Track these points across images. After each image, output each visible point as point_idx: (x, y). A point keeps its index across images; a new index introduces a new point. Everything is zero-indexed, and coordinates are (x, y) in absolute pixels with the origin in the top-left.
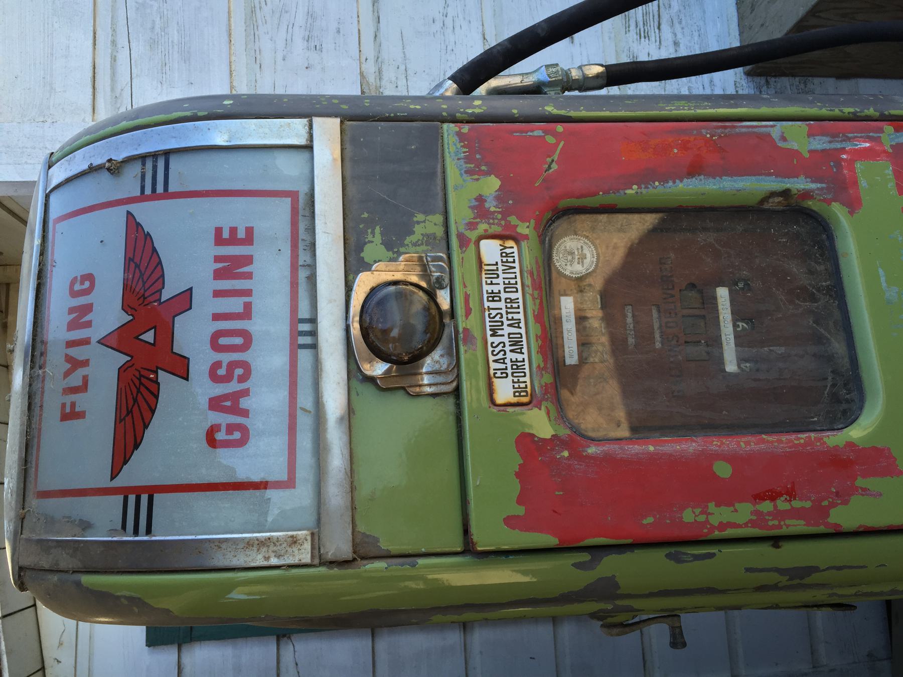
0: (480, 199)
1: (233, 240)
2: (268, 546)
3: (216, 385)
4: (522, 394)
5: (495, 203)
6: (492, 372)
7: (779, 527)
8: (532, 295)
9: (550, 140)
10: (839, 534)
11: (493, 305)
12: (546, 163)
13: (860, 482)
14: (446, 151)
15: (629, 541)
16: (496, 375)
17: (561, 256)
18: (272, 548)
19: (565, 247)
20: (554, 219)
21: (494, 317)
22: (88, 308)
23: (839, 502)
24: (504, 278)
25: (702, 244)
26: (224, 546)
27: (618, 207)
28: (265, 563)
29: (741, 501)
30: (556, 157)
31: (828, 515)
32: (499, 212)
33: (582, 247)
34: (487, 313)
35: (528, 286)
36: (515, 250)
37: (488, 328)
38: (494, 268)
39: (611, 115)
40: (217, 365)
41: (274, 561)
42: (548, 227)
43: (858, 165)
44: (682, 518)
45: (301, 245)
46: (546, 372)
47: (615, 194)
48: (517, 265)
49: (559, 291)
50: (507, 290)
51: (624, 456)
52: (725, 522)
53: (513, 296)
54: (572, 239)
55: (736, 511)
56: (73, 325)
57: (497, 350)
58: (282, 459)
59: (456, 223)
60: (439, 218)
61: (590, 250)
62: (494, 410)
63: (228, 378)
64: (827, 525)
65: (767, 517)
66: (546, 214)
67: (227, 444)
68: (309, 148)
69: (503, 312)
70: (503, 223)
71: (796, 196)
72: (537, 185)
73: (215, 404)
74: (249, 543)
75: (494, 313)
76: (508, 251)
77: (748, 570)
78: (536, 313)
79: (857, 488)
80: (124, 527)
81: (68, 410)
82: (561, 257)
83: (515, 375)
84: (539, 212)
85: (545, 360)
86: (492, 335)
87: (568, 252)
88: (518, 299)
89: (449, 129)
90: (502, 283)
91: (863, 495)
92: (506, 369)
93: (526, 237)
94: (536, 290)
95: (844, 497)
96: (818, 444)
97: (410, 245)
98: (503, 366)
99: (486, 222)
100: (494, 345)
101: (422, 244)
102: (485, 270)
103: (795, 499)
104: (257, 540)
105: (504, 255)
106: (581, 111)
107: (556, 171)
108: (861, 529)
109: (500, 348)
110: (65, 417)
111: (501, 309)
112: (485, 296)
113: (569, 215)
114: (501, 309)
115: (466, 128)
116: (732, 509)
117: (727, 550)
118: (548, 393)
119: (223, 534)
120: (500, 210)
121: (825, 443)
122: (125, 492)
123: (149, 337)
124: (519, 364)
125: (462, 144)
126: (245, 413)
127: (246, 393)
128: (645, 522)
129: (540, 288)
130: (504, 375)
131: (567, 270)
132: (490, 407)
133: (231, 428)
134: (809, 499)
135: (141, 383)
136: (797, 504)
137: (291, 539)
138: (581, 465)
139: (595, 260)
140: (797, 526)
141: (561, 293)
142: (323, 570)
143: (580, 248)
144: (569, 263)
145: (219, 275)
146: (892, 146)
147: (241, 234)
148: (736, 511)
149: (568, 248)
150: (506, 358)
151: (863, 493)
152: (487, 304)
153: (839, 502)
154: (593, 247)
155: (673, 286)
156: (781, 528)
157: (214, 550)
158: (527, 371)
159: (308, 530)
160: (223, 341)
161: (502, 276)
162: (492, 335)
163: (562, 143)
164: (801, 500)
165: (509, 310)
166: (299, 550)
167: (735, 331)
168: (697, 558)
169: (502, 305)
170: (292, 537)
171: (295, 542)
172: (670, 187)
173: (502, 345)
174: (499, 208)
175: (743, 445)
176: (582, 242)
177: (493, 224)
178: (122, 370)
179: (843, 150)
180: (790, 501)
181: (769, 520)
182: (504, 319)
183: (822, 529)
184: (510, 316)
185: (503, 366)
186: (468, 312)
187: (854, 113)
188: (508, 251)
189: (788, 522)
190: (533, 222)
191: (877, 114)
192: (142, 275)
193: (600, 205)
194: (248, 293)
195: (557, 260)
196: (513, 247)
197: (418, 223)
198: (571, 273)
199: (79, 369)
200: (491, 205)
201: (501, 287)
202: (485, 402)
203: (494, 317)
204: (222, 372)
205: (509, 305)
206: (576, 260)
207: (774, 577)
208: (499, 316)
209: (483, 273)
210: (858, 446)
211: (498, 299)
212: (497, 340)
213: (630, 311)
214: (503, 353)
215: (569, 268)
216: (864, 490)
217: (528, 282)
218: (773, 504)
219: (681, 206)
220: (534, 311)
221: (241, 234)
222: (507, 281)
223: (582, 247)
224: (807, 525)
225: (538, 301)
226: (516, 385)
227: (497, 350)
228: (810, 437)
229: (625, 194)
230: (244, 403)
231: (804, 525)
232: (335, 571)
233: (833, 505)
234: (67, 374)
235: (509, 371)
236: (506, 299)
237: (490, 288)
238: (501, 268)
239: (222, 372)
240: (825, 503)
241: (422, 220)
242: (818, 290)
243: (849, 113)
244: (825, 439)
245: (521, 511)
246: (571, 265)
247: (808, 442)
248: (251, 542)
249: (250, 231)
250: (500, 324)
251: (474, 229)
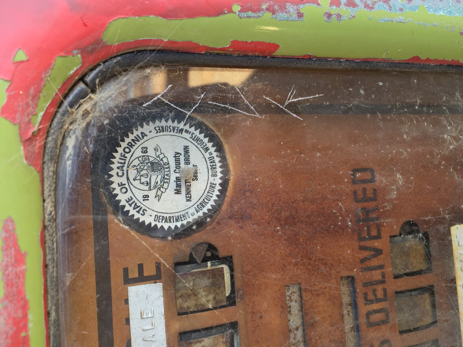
17: (132, 173)
19: (145, 150)
20: (94, 80)
25: (452, 147)
27: (278, 53)
33: (186, 149)
42: (71, 105)
47: (274, 12)
49: (126, 271)
54: (162, 129)
61: (207, 155)
66: (59, 61)
82: (131, 178)
84: (28, 54)
87: (152, 163)
113: (142, 68)
131: (149, 212)
137: (297, 11)
139: (218, 181)
141: (131, 276)
143: (182, 152)
144: (152, 194)
149: (151, 153)
154: (212, 150)
155: (379, 231)
172: (401, 10)
176: (188, 136)
193: (234, 43)
195: (121, 185)
198: (157, 218)
199: (231, 84)
206: (173, 185)
213: (295, 297)
215: (152, 203)
219: (416, 58)
223: (186, 149)
229: (300, 15)
246: (158, 197)
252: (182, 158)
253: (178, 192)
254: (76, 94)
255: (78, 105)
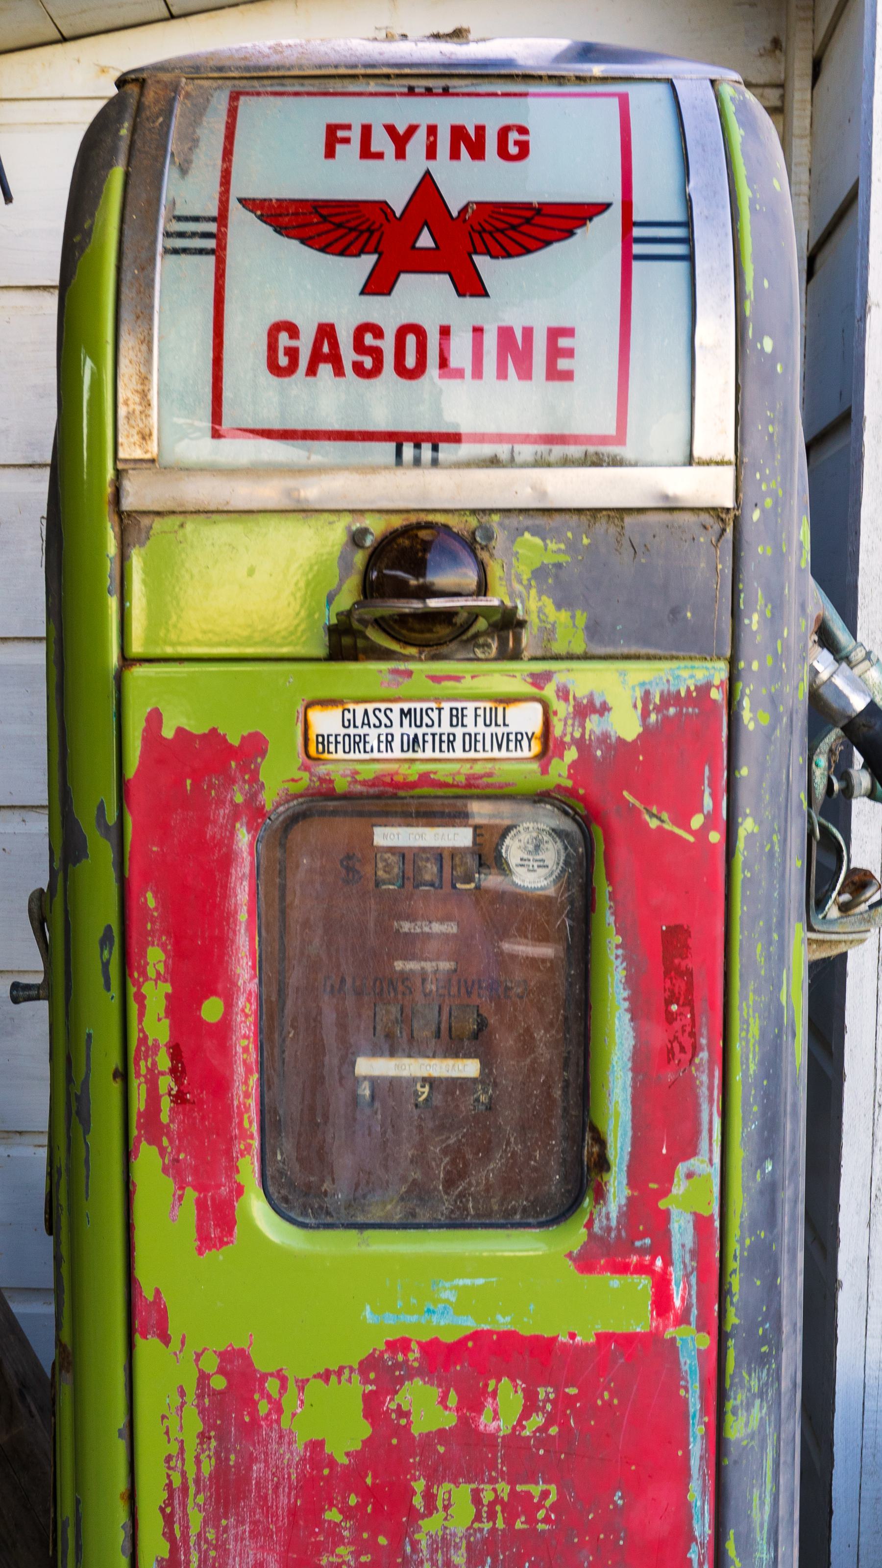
0: (604, 709)
1: (554, 353)
2: (141, 404)
3: (352, 333)
4: (320, 746)
5: (598, 731)
6: (351, 706)
7: (138, 1075)
8: (459, 773)
9: (697, 822)
10: (128, 1155)
11: (446, 715)
12: (659, 811)
13: (191, 1195)
14: (682, 664)
15: (127, 874)
16: (346, 712)
18: (138, 408)
21: (427, 714)
22: (477, 152)
23: (166, 1161)
24: (484, 735)
26: (144, 348)
28: (121, 400)
29: (173, 1028)
30: (668, 826)
31: (150, 1143)
32: (583, 735)
34: (433, 705)
35: (471, 768)
36: (526, 754)
37: (412, 705)
38: (500, 721)
39: (406, 664)
40: (378, 333)
41: (122, 411)
43: (644, 1282)
44: (153, 945)
45: (542, 448)
46: (350, 783)
48: (504, 754)
50: (467, 737)
51: (234, 878)
52: (146, 1002)
53: (458, 744)
55: (159, 1020)
56: (458, 133)
57: (381, 716)
58: (249, 420)
59: (568, 670)
60: (579, 647)
62: (301, 710)
63: (359, 347)
64: (138, 1140)
65: (150, 1060)
67: (272, 347)
68: (690, 460)
69: (436, 729)
70: (567, 739)
71: (599, 1179)
72: (625, 794)
73: (326, 332)
74: (145, 379)
75: (434, 715)
76: (525, 742)
77: (89, 1036)
78: (432, 776)
79: (182, 1188)
80: (179, 219)
81: (340, 134)
83: (347, 738)
85: (364, 783)
86: (402, 711)
88: (454, 750)
89: (719, 672)
90: (476, 730)
91: (174, 1195)
92: (355, 726)
93: (545, 771)
94: (467, 779)
95: (174, 1169)
96: (242, 1147)
97: (540, 604)
98: (359, 723)
99: (568, 714)
100: (388, 712)
101: (541, 621)
102: (496, 709)
103: (172, 1101)
104: (149, 390)
105: (519, 737)
106: (743, 872)
107: (647, 824)
108: (131, 1188)
109: (385, 720)
110: (332, 130)
111: (440, 725)
112: (459, 705)
114: (440, 725)
115: (716, 695)
116: (162, 1014)
117: (116, 1003)
118: (321, 783)
119: (159, 346)
120: (587, 737)
121: (243, 1156)
122: (222, 218)
123: (425, 240)
124: (361, 745)
125: (692, 688)
126: (312, 371)
127: (339, 371)
128: (149, 895)
129: (469, 785)
130: (346, 724)
132: (303, 700)
133: (293, 353)
134: (172, 1121)
135: (362, 232)
136: (166, 1104)
138: (224, 818)
140: (139, 1101)
142: (110, 474)
145: (505, 334)
146: (673, 1339)
147: (563, 364)
148: (159, 1020)
150: (370, 727)
151: (177, 1196)
152: (447, 706)
153: (166, 1161)
156: (136, 1077)
157: (139, 335)
158: (351, 756)
159: (158, 455)
160: (411, 340)
161: (488, 731)
162: (402, 711)
163: (691, 839)
164: (171, 1109)
165: (437, 738)
166: (135, 444)
167: (414, 1080)
168: (106, 965)
169: (446, 728)
170: (150, 435)
171: (144, 438)
173: (389, 724)
174: (590, 736)
175: (244, 1043)
177: (565, 724)
178: (383, 206)
179: (668, 1262)
180: (170, 1095)
181: (146, 1061)
182: (424, 729)
183: (134, 1132)
184: (429, 738)
185: (359, 723)
186: (436, 679)
187: (729, 1291)
188: (525, 742)
189: (144, 1087)
190: (569, 783)
191: (728, 1328)
192: (514, 227)
194: (478, 373)
196: (530, 750)
197: (573, 617)
200: (593, 724)
201: (471, 729)
202: (309, 696)
203: (427, 714)
204: (369, 339)
205: (445, 738)
206: (525, 856)
207: (79, 1077)
208: (430, 723)
209: (493, 705)
210: (237, 1201)
211: (455, 722)
212: (395, 716)
214: (377, 724)
216: (181, 1198)
217: (478, 768)
218: (167, 1070)
220: (435, 773)
221: (563, 364)
222: (480, 738)
224: (140, 1114)
225: (450, 780)
226: (332, 739)
227: (381, 716)
228: (252, 1137)
230: (325, 369)
231: (139, 1109)
232: (109, 490)
233: (162, 1152)
234: (391, 129)
235: (352, 731)
236: (454, 735)
237: (470, 713)
238: (500, 731)
239: (369, 339)
240: (165, 1142)
241: (576, 623)
242: (461, 1195)
243: (730, 1284)
244: (248, 1158)
245: (168, 732)
247: (245, 1135)
248: (146, 382)
249: (568, 376)
250: (418, 723)
251: (558, 696)
252: (541, 864)
253: (522, 859)
254: (696, 1108)
255: (563, 799)
